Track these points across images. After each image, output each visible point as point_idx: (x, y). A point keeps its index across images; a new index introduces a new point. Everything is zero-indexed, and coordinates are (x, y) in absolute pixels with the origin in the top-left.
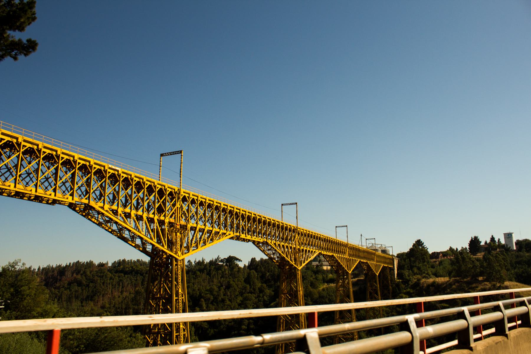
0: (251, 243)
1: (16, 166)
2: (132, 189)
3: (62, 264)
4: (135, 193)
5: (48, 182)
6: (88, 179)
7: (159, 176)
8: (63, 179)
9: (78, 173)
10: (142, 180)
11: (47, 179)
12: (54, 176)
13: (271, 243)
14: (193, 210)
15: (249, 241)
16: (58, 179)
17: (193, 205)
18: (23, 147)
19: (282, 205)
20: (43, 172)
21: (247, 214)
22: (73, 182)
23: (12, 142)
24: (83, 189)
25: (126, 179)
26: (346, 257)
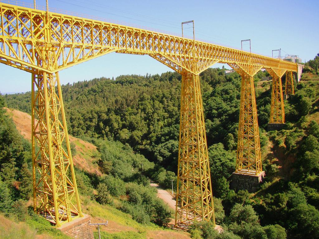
0: (148, 56)
1: (60, 31)
2: (125, 35)
3: (128, 75)
4: (135, 38)
5: (79, 37)
6: (100, 33)
7: (46, 8)
8: (86, 35)
9: (94, 30)
10: (144, 32)
11: (78, 36)
12: (81, 34)
13: (164, 54)
14: (167, 44)
15: (226, 63)
16: (84, 35)
17: (172, 42)
18: (18, 13)
19: (182, 23)
20: (75, 32)
21: (222, 48)
22: (101, 37)
23: (10, 10)
24: (98, 39)
25: (121, 30)
26: (249, 64)
